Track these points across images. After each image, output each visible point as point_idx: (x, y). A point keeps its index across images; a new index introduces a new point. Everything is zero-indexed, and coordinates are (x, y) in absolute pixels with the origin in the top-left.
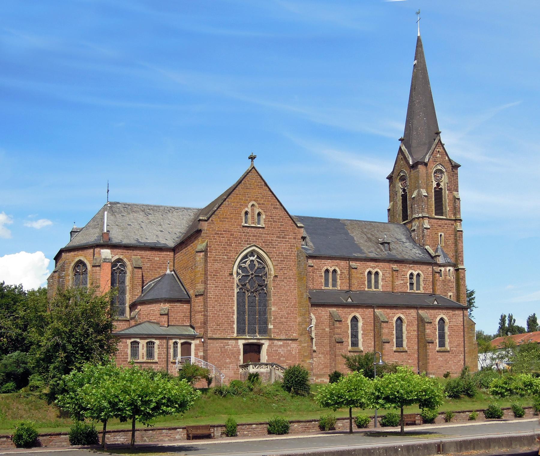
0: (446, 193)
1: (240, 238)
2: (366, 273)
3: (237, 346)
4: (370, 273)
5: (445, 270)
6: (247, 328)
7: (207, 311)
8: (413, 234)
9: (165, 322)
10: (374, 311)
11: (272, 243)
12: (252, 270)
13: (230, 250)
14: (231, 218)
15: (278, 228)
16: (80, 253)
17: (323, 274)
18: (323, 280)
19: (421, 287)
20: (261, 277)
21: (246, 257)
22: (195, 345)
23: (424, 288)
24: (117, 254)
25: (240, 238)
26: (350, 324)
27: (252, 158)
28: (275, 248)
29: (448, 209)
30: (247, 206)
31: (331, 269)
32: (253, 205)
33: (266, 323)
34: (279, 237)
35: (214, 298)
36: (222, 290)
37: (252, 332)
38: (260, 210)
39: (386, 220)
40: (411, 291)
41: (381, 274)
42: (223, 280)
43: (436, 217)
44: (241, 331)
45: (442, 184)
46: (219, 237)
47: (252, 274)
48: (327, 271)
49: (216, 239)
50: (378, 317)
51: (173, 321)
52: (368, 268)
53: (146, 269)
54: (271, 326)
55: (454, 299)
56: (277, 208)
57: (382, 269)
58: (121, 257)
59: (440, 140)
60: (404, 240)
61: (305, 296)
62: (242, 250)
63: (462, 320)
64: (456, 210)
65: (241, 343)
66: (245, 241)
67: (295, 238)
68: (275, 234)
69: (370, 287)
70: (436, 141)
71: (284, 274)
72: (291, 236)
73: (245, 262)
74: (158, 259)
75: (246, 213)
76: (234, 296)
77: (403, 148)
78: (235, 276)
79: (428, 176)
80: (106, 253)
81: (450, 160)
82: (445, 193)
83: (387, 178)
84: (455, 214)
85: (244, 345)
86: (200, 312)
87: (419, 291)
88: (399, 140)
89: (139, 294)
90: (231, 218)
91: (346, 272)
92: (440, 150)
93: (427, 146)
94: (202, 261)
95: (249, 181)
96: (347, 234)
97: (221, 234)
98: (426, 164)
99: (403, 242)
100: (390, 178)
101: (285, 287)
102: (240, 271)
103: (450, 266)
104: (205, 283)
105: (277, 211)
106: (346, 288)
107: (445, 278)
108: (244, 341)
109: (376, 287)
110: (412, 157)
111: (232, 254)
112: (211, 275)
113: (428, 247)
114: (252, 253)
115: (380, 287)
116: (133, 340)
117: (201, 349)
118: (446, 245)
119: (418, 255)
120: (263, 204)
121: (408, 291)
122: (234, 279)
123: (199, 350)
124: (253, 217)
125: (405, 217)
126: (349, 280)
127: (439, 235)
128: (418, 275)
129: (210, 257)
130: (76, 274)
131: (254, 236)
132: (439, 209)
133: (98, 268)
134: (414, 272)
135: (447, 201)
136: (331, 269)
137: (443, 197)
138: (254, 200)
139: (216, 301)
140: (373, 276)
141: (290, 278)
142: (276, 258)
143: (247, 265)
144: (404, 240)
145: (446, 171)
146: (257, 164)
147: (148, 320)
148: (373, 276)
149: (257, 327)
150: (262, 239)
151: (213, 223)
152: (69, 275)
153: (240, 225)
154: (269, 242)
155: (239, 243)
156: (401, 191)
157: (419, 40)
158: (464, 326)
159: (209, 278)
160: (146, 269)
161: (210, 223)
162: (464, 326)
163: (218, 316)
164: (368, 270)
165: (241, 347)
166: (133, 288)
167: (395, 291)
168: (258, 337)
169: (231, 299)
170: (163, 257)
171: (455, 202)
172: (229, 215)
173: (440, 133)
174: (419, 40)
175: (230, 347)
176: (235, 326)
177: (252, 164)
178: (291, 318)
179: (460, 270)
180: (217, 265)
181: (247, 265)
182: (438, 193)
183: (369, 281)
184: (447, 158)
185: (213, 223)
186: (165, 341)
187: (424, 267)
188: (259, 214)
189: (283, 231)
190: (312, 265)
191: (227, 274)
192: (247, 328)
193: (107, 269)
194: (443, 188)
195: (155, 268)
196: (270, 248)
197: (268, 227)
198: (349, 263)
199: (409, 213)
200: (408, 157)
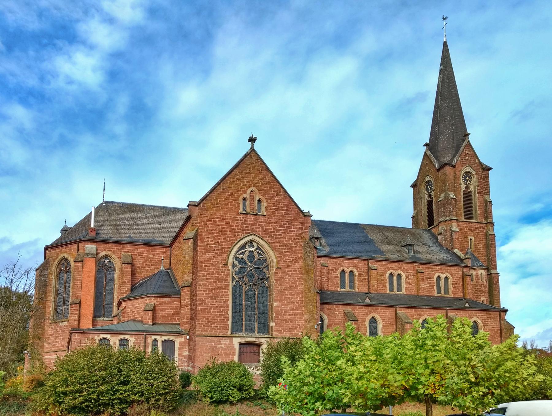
0: (476, 198)
1: (236, 226)
2: (387, 275)
3: (231, 345)
4: (391, 275)
5: (477, 273)
6: (244, 324)
7: (195, 305)
8: (439, 237)
9: (149, 319)
10: (396, 312)
11: (274, 232)
12: (251, 262)
13: (225, 239)
14: (227, 204)
15: (281, 216)
16: (65, 249)
17: (339, 275)
18: (339, 282)
19: (450, 291)
20: (262, 269)
21: (243, 247)
22: (180, 343)
23: (453, 292)
24: (105, 250)
25: (236, 226)
26: (368, 326)
27: (252, 140)
28: (278, 238)
29: (479, 212)
30: (245, 192)
31: (348, 270)
32: (252, 191)
33: (267, 320)
34: (283, 227)
35: (204, 291)
36: (214, 282)
37: (250, 329)
38: (261, 197)
39: (410, 226)
40: (438, 295)
41: (404, 276)
42: (216, 272)
43: (465, 220)
44: (236, 329)
45: (472, 188)
46: (212, 224)
47: (251, 266)
48: (343, 272)
49: (208, 227)
50: (400, 318)
51: (160, 318)
52: (389, 270)
53: (138, 267)
54: (272, 324)
55: (487, 303)
56: (281, 195)
57: (406, 271)
58: (109, 253)
59: (469, 141)
60: (430, 244)
61: (312, 290)
62: (238, 240)
63: (498, 324)
64: (487, 213)
65: (236, 341)
66: (243, 230)
67: (301, 228)
68: (278, 223)
69: (391, 289)
70: (465, 143)
71: (288, 266)
72: (297, 225)
73: (243, 253)
74: (152, 256)
75: (244, 199)
76: (228, 290)
77: (429, 153)
78: (230, 267)
79: (456, 178)
80: (91, 248)
81: (480, 163)
82: (475, 196)
83: (411, 186)
84: (486, 218)
85: (241, 344)
86: (187, 306)
87: (447, 295)
88: (425, 145)
89: (128, 292)
90: (227, 204)
91: (365, 274)
92: (469, 153)
93: (454, 150)
94: (191, 249)
95: (248, 165)
96: (366, 237)
97: (214, 221)
98: (454, 166)
99: (429, 246)
100: (414, 186)
101: (289, 280)
102: (236, 263)
103: (482, 269)
104: (194, 273)
105: (281, 198)
106: (365, 290)
107: (477, 282)
108: (239, 340)
109: (399, 289)
110: (437, 158)
111: (228, 244)
112: (201, 266)
113: (457, 250)
114: (251, 242)
115: (403, 290)
116: (102, 336)
117: (186, 347)
118: (477, 250)
119: (446, 258)
120: (264, 190)
121: (436, 295)
122: (229, 270)
123: (183, 348)
124: (252, 205)
125: (431, 222)
126: (369, 282)
127: (469, 238)
128: (446, 278)
129: (201, 246)
130: (60, 272)
131: (253, 224)
132: (469, 214)
133: (80, 264)
134: (441, 275)
135: (478, 204)
136: (348, 270)
137: (474, 210)
138: (254, 186)
139: (206, 294)
140: (395, 279)
141: (296, 271)
142: (279, 249)
143: (245, 257)
144: (430, 244)
145: (476, 174)
146: (256, 146)
147: (133, 318)
148: (395, 279)
149: (256, 324)
150: (262, 228)
151: (205, 209)
152: (52, 274)
153: (237, 213)
154: (271, 232)
155: (235, 232)
156: (426, 196)
157: (445, 44)
158: (501, 330)
159: (199, 269)
160: (138, 267)
161: (201, 209)
162: (501, 330)
163: (209, 311)
164: (389, 272)
165: (237, 347)
166: (121, 285)
167: (421, 294)
168: (257, 335)
169: (225, 292)
170: (158, 254)
171: (486, 205)
172: (223, 201)
173: (469, 134)
174: (445, 44)
175: (223, 346)
176: (230, 323)
177: (252, 145)
178: (297, 315)
179: (493, 275)
180: (209, 256)
181: (245, 257)
182: (468, 196)
183: (391, 284)
184: (477, 161)
185: (205, 209)
186: (142, 338)
187: (454, 269)
188: (259, 201)
189: (288, 220)
190: (326, 265)
191: (220, 264)
192: (244, 324)
193: (91, 264)
194: (473, 191)
195: (148, 265)
196: (272, 237)
197: (270, 215)
198: (368, 264)
199: (435, 217)
200: (434, 161)
